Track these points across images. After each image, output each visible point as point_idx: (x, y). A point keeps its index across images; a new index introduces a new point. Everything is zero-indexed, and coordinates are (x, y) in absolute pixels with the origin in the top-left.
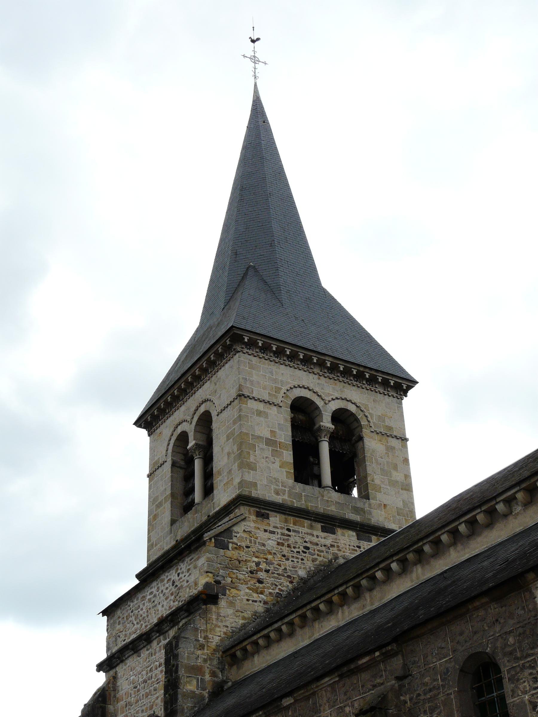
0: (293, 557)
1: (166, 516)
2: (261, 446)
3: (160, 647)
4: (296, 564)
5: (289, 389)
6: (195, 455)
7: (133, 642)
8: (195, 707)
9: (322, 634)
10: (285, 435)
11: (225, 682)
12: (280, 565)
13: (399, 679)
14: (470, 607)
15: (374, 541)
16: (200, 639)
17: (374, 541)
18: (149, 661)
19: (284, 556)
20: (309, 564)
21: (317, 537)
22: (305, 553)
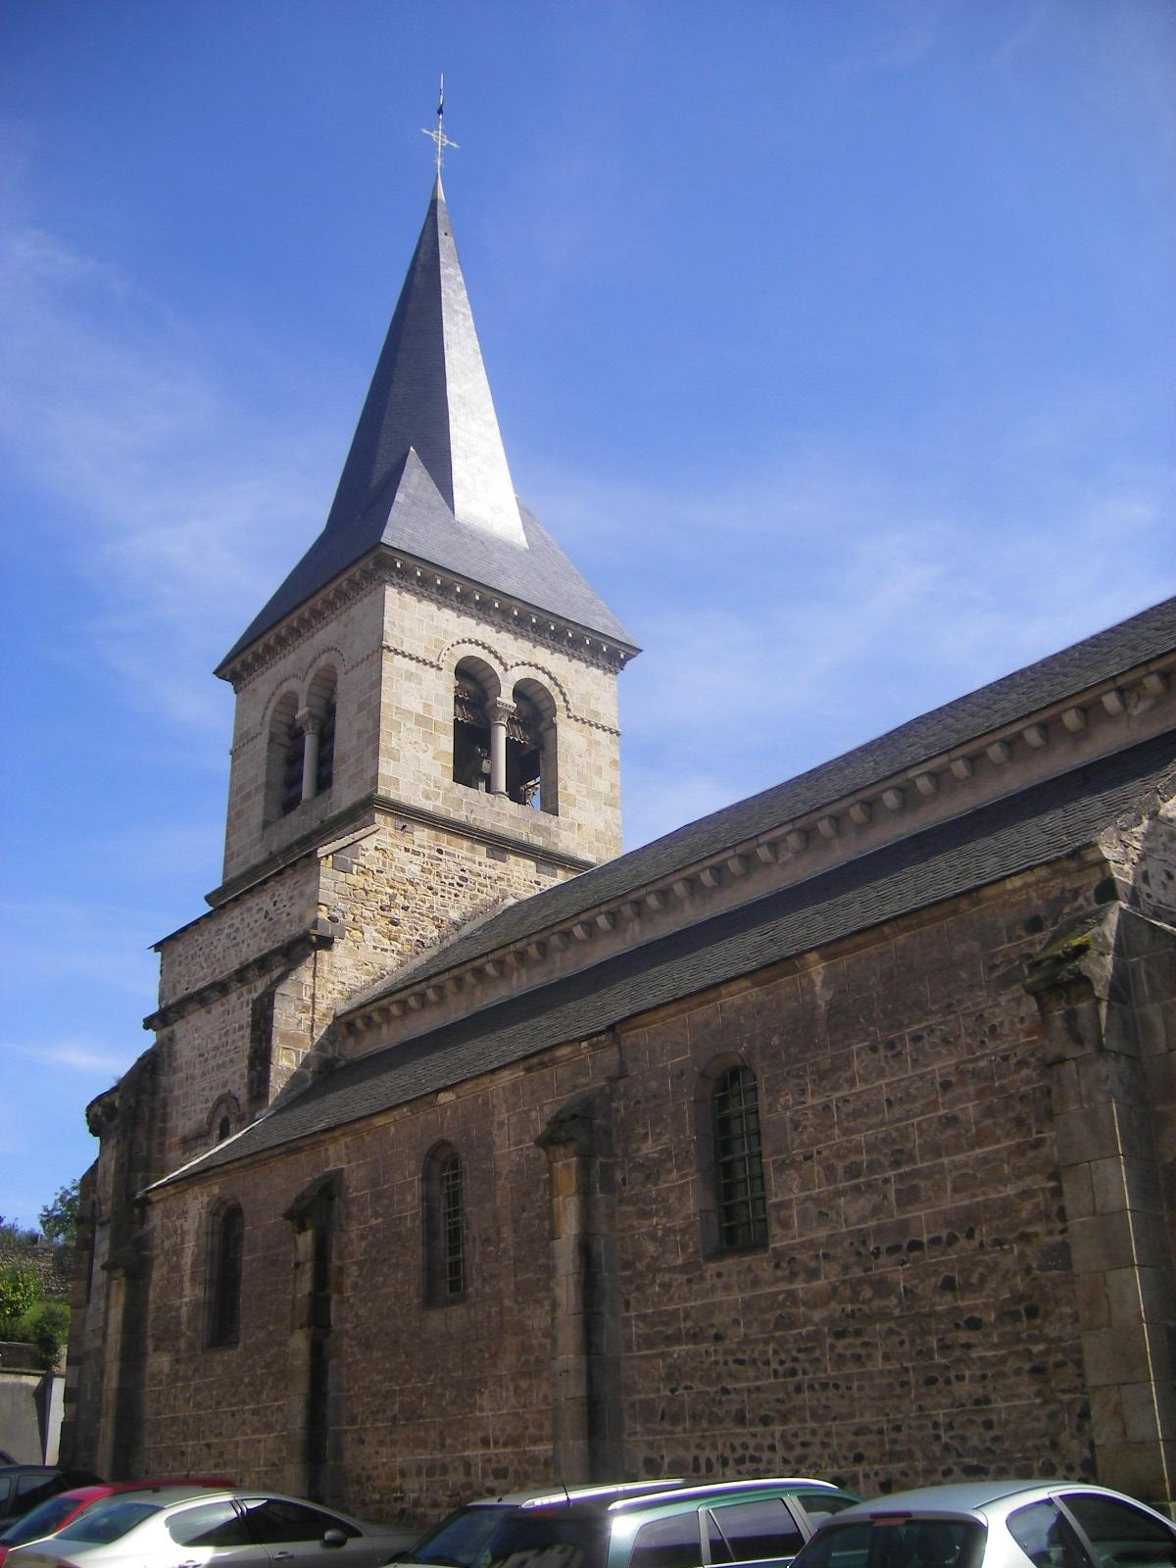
0: (443, 890)
1: (256, 813)
2: (409, 725)
3: (242, 1003)
4: (446, 901)
5: (460, 641)
6: (305, 729)
7: (200, 992)
8: (293, 1090)
9: (487, 1005)
10: (445, 712)
11: (336, 1060)
12: (424, 902)
13: (609, 1079)
14: (724, 992)
15: (561, 877)
16: (304, 998)
17: (561, 877)
18: (224, 1021)
19: (430, 888)
20: (466, 902)
21: (480, 864)
22: (462, 886)
